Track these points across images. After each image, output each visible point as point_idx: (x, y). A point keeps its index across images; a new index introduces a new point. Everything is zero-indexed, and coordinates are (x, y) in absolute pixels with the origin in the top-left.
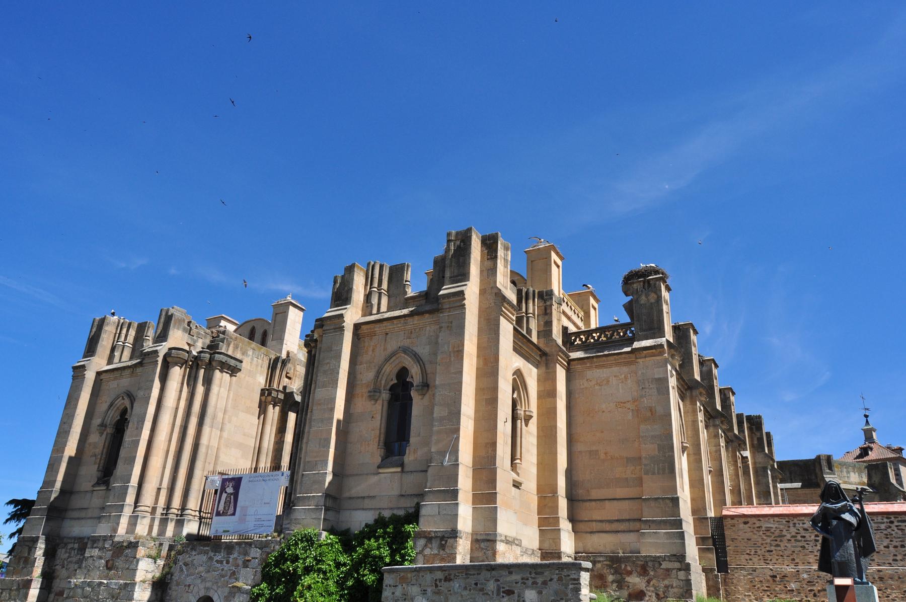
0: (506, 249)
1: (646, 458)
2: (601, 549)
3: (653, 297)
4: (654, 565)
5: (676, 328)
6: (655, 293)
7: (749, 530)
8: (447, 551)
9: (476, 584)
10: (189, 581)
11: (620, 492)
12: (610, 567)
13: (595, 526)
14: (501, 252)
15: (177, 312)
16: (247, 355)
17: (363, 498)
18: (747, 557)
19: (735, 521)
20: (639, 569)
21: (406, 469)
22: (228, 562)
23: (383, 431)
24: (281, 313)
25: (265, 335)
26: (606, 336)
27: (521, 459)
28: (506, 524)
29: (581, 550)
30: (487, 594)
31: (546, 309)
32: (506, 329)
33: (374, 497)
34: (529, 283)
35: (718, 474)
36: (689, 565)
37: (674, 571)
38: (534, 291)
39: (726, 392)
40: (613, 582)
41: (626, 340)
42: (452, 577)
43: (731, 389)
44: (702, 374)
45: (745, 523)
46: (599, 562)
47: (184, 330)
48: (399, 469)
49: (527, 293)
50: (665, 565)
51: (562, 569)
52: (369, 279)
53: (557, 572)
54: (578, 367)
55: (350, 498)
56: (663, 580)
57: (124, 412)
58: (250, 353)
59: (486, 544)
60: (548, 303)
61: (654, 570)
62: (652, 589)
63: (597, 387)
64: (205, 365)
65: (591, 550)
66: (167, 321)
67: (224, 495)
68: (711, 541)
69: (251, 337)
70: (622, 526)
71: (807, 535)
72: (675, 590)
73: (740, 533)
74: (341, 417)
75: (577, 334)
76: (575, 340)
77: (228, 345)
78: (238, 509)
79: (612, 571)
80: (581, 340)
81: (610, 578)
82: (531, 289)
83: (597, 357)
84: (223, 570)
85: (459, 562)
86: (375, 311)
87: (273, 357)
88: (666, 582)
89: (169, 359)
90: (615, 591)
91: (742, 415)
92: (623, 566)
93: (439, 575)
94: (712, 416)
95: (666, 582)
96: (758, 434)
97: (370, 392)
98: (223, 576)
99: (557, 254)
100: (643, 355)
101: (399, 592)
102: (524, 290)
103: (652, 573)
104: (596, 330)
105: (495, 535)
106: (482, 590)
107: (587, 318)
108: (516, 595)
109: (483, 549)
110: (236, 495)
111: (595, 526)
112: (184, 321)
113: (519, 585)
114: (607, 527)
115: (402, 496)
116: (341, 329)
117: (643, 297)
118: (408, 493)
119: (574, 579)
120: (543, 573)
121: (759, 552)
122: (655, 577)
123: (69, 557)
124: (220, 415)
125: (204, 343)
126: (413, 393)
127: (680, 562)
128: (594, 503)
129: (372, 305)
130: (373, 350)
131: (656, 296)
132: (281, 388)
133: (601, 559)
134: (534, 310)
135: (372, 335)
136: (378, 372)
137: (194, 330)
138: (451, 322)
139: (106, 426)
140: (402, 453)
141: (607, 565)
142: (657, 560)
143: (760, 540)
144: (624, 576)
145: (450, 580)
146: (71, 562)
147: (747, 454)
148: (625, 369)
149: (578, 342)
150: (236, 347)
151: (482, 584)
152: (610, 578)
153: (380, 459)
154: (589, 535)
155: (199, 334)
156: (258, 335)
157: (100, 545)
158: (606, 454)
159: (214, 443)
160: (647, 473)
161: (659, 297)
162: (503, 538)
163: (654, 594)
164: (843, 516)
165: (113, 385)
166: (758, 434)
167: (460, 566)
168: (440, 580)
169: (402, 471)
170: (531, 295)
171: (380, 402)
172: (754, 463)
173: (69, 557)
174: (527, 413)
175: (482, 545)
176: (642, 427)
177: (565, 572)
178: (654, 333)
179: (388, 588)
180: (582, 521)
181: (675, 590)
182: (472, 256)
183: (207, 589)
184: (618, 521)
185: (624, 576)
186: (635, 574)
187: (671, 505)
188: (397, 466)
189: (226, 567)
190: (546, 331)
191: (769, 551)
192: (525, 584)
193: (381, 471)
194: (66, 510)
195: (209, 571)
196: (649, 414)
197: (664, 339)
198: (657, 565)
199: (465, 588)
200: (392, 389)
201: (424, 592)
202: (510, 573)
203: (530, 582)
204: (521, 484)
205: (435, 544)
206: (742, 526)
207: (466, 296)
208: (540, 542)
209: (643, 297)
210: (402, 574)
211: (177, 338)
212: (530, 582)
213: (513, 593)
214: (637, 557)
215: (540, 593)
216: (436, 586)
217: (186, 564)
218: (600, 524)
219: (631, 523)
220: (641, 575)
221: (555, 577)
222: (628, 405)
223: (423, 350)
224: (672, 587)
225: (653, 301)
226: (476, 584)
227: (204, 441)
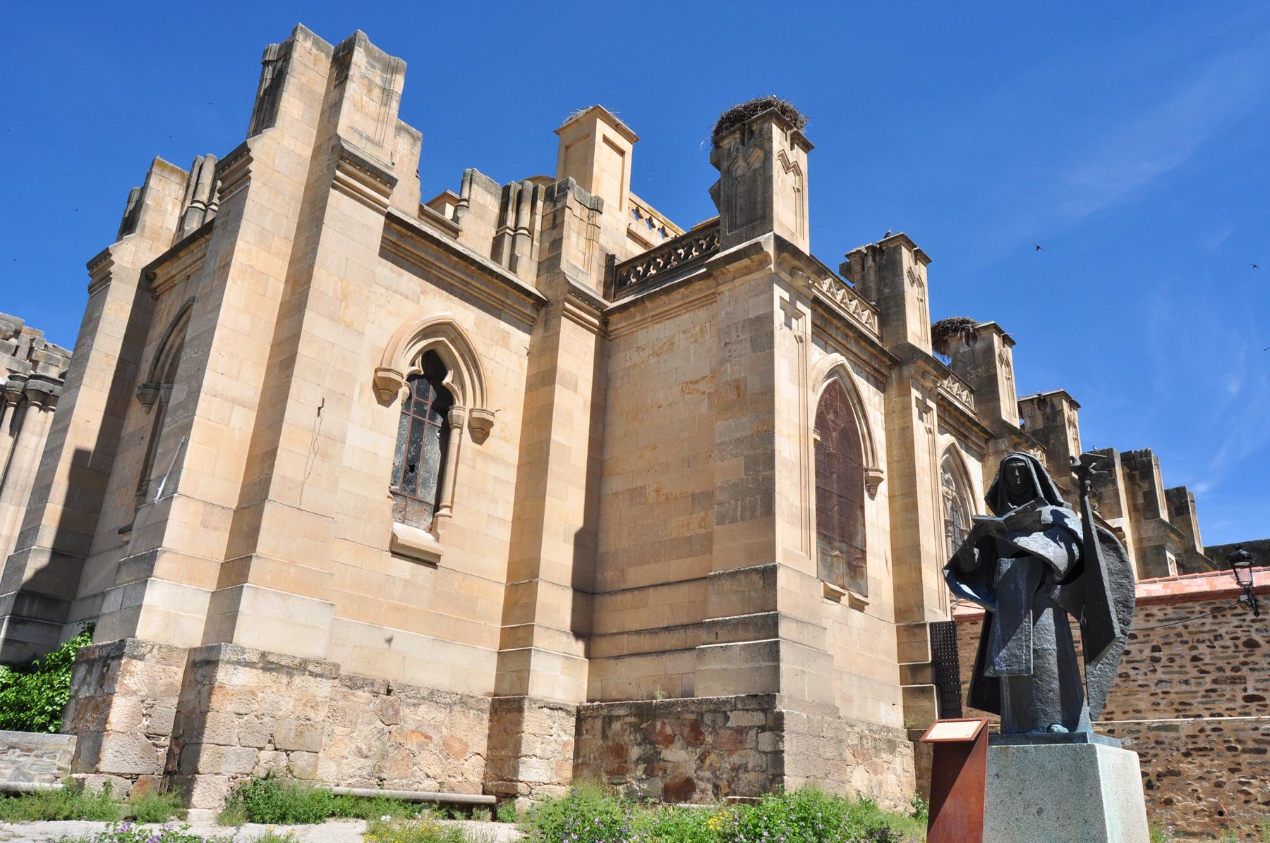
1: (722, 488)
2: (632, 691)
6: (761, 147)
12: (636, 728)
13: (628, 644)
20: (686, 731)
29: (599, 696)
31: (555, 218)
36: (780, 716)
37: (752, 733)
39: (1056, 401)
40: (637, 762)
43: (1065, 395)
46: (618, 718)
49: (520, 193)
50: (736, 719)
54: (617, 323)
56: (731, 753)
60: (559, 206)
61: (715, 732)
62: (708, 774)
63: (653, 360)
65: (614, 694)
68: (929, 673)
70: (672, 640)
71: (1133, 648)
74: (90, 444)
81: (635, 752)
83: (650, 297)
88: (736, 759)
90: (641, 780)
91: (1110, 452)
92: (659, 726)
95: (736, 759)
96: (1145, 486)
103: (709, 739)
111: (628, 644)
114: (647, 643)
117: (741, 163)
127: (764, 711)
128: (628, 596)
133: (622, 712)
134: (532, 223)
141: (631, 724)
142: (720, 709)
144: (660, 747)
147: (1124, 522)
148: (702, 314)
154: (612, 662)
158: (657, 491)
160: (721, 521)
163: (710, 786)
164: (1022, 542)
166: (1145, 486)
170: (528, 196)
172: (1139, 541)
176: (721, 425)
178: (754, 229)
180: (604, 635)
181: (751, 776)
185: (660, 747)
186: (679, 743)
196: (733, 396)
198: (720, 720)
204: (438, 557)
208: (499, 678)
209: (741, 163)
214: (685, 704)
218: (634, 638)
219: (689, 632)
220: (689, 744)
222: (702, 386)
224: (746, 771)
225: (757, 165)
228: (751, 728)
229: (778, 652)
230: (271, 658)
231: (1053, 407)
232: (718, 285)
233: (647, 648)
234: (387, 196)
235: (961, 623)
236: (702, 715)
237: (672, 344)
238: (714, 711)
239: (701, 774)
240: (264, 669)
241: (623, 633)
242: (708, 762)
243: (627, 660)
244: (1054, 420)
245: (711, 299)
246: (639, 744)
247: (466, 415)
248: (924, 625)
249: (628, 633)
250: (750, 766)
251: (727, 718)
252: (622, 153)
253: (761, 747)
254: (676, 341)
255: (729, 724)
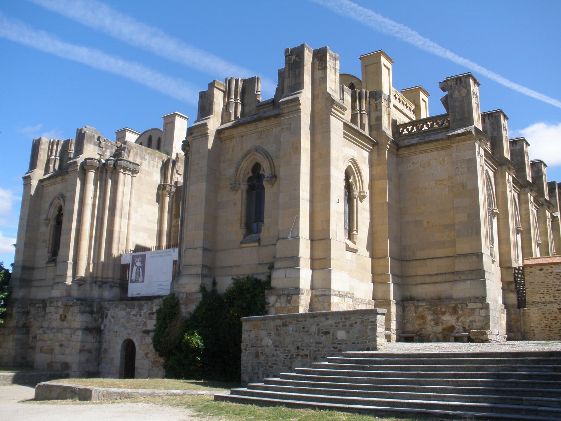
0: (335, 59)
3: (464, 92)
4: (462, 307)
5: (485, 117)
6: (466, 88)
7: (543, 275)
8: (292, 304)
9: (304, 328)
10: (116, 328)
11: (439, 252)
12: (429, 309)
14: (330, 62)
15: (88, 130)
16: (145, 159)
17: (231, 267)
18: (541, 296)
19: (533, 269)
20: (451, 310)
21: (263, 243)
22: (140, 316)
23: (243, 214)
24: (169, 122)
25: (159, 140)
26: (437, 124)
27: (357, 232)
28: (340, 281)
30: (311, 334)
32: (336, 127)
33: (239, 266)
34: (364, 84)
35: (525, 234)
36: (488, 304)
37: (477, 310)
38: (366, 92)
39: (539, 165)
40: (431, 320)
41: (444, 128)
42: (287, 323)
44: (512, 153)
45: (541, 270)
46: (421, 306)
47: (95, 144)
48: (257, 244)
50: (471, 306)
51: (364, 315)
52: (227, 94)
53: (360, 317)
55: (222, 267)
56: (469, 316)
57: (60, 209)
58: (147, 157)
59: (323, 298)
60: (378, 101)
61: (462, 309)
62: (460, 324)
63: (421, 169)
64: (109, 171)
66: (81, 137)
67: (135, 268)
69: (149, 145)
70: (439, 279)
72: (478, 324)
73: (537, 278)
75: (405, 125)
76: (403, 131)
77: (129, 152)
78: (146, 277)
79: (431, 312)
80: (407, 130)
81: (429, 318)
82: (364, 90)
84: (137, 321)
85: (302, 311)
86: (232, 118)
87: (166, 159)
88: (471, 318)
89: (85, 167)
91: (554, 182)
92: (439, 309)
93: (279, 322)
94: (521, 184)
95: (471, 318)
97: (231, 184)
98: (139, 325)
99: (388, 58)
100: (456, 141)
101: (253, 335)
102: (358, 91)
103: (460, 312)
104: (425, 121)
105: (330, 291)
106: (307, 332)
107: (417, 111)
108: (331, 334)
109: (320, 302)
110: (143, 267)
112: (94, 137)
113: (333, 327)
115: (260, 264)
116: (206, 135)
117: (456, 92)
118: (264, 262)
119: (372, 322)
120: (349, 318)
121: (550, 291)
122: (462, 315)
123: (38, 313)
124: (126, 208)
125: (111, 152)
126: (265, 184)
127: (482, 303)
129: (230, 114)
130: (233, 151)
131: (466, 91)
132: (173, 183)
135: (231, 138)
136: (237, 168)
137: (103, 144)
138: (290, 124)
139: (49, 220)
140: (259, 231)
141: (427, 308)
143: (551, 282)
145: (286, 325)
146: (39, 316)
148: (443, 153)
149: (405, 132)
150: (136, 154)
151: (307, 328)
152: (429, 318)
153: (242, 237)
154: (414, 287)
155: (106, 145)
156: (154, 142)
157: (55, 304)
158: (428, 222)
159: (124, 229)
161: (469, 93)
162: (337, 293)
165: (51, 189)
167: (302, 314)
168: (280, 326)
169: (259, 245)
171: (240, 192)
173: (38, 313)
174: (362, 194)
175: (320, 299)
177: (366, 317)
179: (246, 332)
182: (305, 68)
183: (129, 334)
184: (437, 274)
185: (440, 316)
186: (448, 314)
187: (476, 260)
188: (255, 242)
189: (140, 319)
190: (376, 125)
191: (558, 290)
192: (337, 326)
193: (243, 245)
194: (31, 281)
195: (128, 322)
197: (473, 126)
198: (464, 306)
199: (296, 331)
200: (250, 179)
201: (269, 335)
202: (327, 319)
203: (340, 325)
205: (283, 299)
206: (538, 272)
207: (301, 102)
209: (456, 92)
210: (254, 322)
211: (90, 151)
212: (340, 325)
213: (329, 333)
215: (348, 332)
216: (277, 330)
217: (113, 317)
221: (359, 321)
223: (271, 148)
224: (475, 322)
225: (464, 95)
226: (304, 328)
227: (116, 228)
228: (477, 308)
229: (485, 283)
230: (341, 293)
231: (538, 167)
232: (451, 144)
233: (429, 281)
234: (343, 114)
235: (526, 267)
236: (457, 304)
237: (430, 163)
238: (462, 303)
239: (457, 324)
240: (340, 296)
241: (417, 276)
242: (460, 320)
243: (421, 286)
244: (538, 173)
245: (448, 147)
246: (431, 315)
247: (358, 194)
248: (512, 268)
249: (419, 276)
250: (477, 320)
251: (467, 306)
252: (388, 69)
253: (481, 314)
254: (431, 165)
255: (468, 307)
